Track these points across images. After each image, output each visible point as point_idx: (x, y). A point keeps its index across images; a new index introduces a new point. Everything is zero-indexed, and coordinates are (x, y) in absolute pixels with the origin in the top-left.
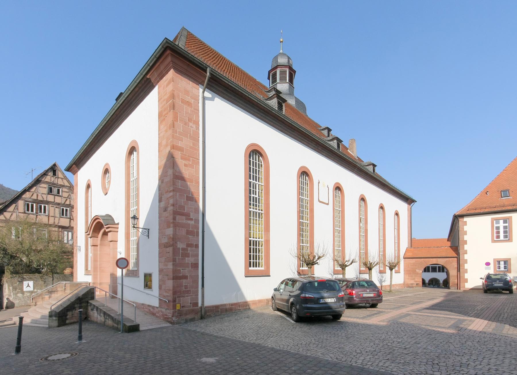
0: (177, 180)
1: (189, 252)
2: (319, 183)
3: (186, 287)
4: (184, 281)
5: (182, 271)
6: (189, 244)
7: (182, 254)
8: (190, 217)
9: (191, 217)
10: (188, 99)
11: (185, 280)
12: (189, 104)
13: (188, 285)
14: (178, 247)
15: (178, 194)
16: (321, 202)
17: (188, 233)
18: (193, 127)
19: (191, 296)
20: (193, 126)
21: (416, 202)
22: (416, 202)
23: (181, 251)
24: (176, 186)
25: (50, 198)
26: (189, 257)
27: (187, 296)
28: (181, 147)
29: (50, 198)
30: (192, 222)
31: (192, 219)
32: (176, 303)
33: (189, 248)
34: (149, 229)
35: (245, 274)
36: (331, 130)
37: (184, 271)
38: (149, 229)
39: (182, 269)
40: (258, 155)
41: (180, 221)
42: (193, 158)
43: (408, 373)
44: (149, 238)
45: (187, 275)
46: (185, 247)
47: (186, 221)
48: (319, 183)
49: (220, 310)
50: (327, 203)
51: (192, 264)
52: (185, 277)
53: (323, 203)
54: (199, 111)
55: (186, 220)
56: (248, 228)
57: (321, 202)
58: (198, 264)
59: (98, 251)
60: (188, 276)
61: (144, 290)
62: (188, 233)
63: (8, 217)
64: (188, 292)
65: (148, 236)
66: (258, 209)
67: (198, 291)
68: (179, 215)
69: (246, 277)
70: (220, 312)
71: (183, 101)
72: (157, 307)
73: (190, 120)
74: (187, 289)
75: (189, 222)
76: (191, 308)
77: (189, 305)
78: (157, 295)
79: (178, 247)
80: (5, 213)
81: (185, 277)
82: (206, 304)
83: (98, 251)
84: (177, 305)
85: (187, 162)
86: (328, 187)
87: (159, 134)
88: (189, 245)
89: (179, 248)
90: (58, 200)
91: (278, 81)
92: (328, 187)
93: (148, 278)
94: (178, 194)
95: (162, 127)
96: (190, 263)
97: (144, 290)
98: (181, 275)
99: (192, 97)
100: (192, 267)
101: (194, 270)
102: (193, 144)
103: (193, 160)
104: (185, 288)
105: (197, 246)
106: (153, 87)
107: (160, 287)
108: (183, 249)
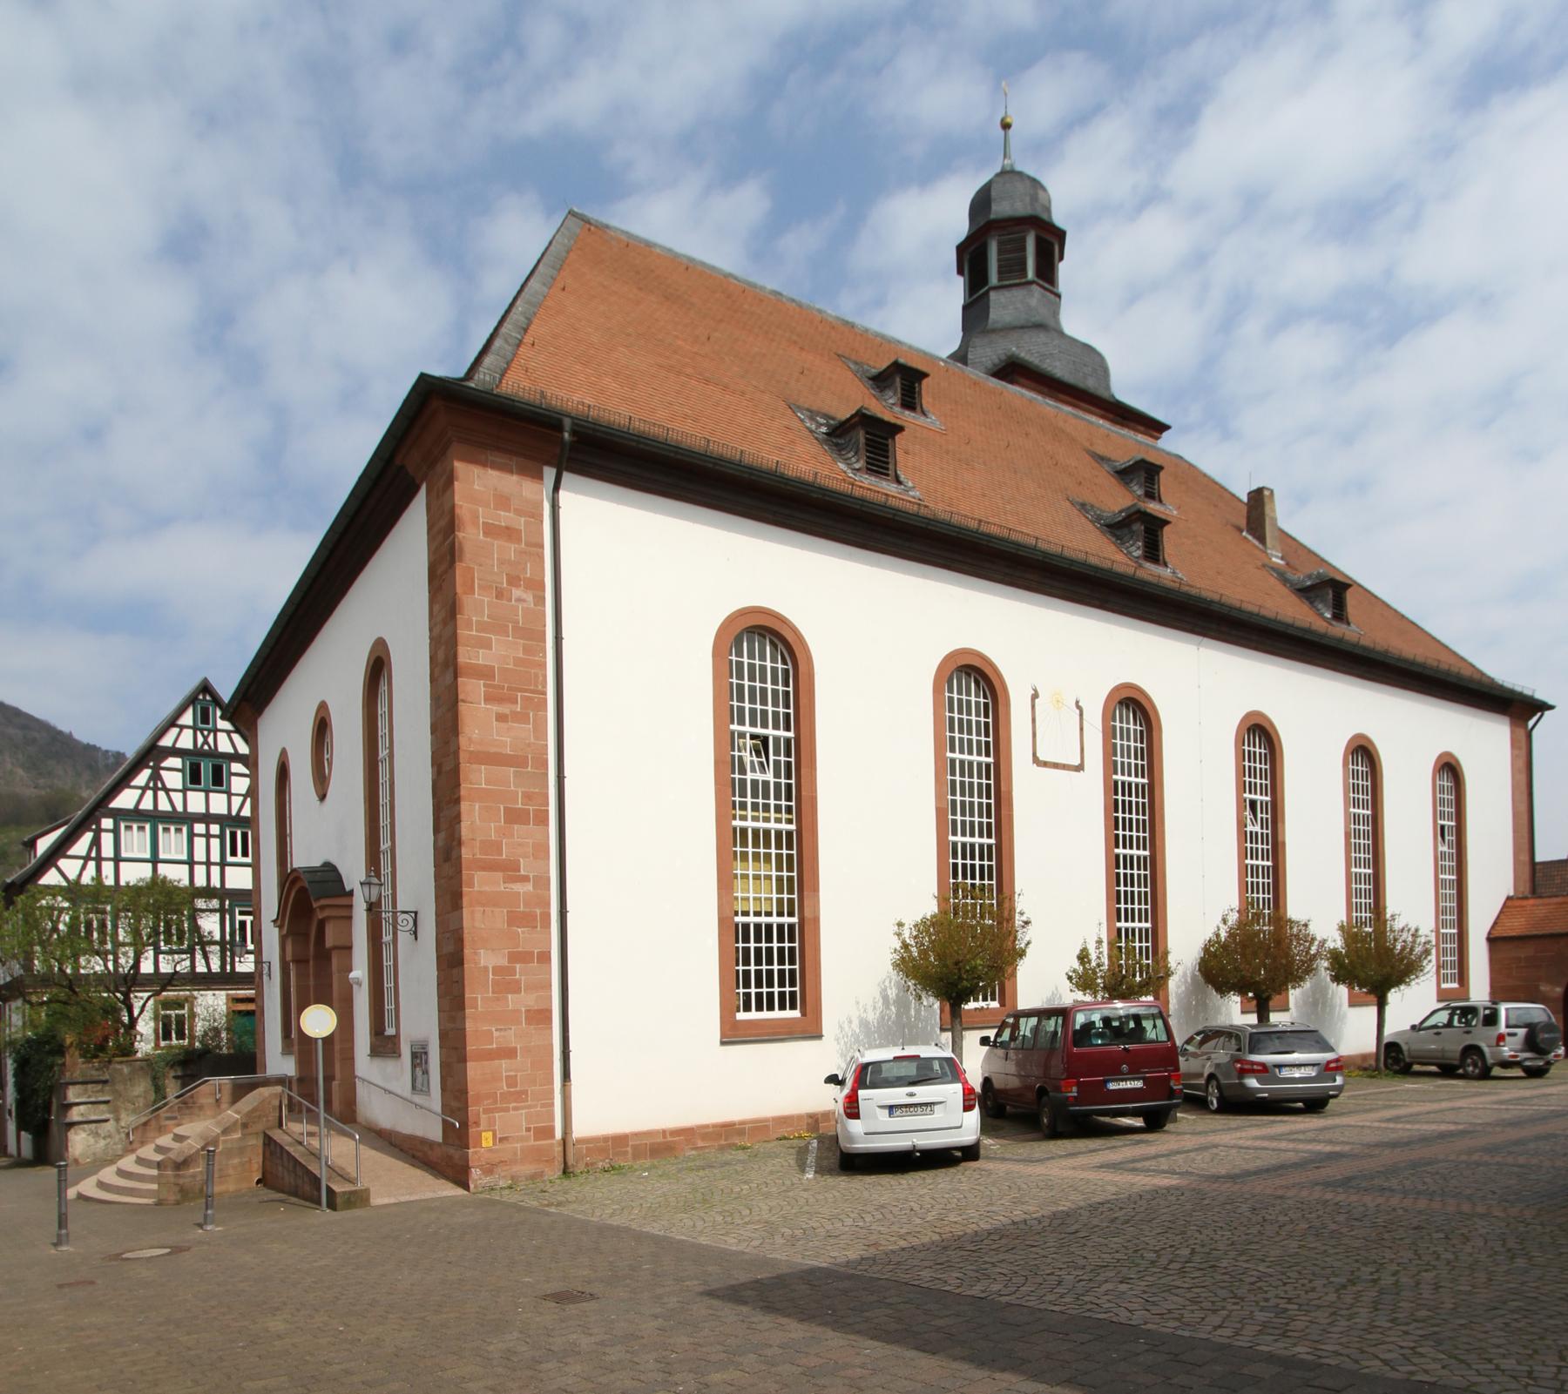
0: (474, 766)
1: (518, 976)
2: (1035, 696)
3: (512, 1081)
4: (504, 1063)
5: (496, 1034)
6: (519, 953)
7: (495, 983)
8: (519, 871)
9: (522, 872)
10: (505, 518)
11: (508, 1061)
12: (510, 533)
13: (519, 1074)
14: (482, 963)
15: (477, 807)
16: (1045, 764)
17: (515, 919)
18: (524, 601)
19: (529, 1107)
20: (524, 596)
21: (1551, 707)
22: (1551, 707)
23: (491, 976)
24: (471, 783)
25: (196, 802)
26: (518, 991)
27: (516, 1109)
28: (486, 666)
29: (196, 802)
30: (529, 887)
31: (525, 879)
32: (481, 1128)
33: (518, 966)
34: (416, 913)
35: (723, 1035)
36: (1161, 468)
37: (502, 1033)
38: (416, 913)
39: (496, 1030)
40: (772, 643)
41: (487, 889)
42: (526, 691)
43: (1400, 1368)
44: (416, 939)
45: (513, 1045)
46: (504, 962)
47: (507, 885)
48: (1035, 696)
49: (629, 1149)
50: (1077, 762)
51: (528, 1011)
52: (510, 1053)
53: (1056, 766)
54: (542, 546)
55: (504, 882)
56: (726, 881)
57: (1045, 764)
58: (550, 1011)
59: (311, 978)
60: (516, 1048)
61: (413, 1094)
62: (515, 919)
63: (72, 876)
64: (520, 1096)
65: (415, 933)
66: (772, 819)
67: (552, 1091)
68: (484, 869)
69: (723, 1043)
70: (630, 1156)
71: (490, 530)
72: (439, 1144)
73: (514, 581)
74: (516, 1086)
75: (518, 887)
76: (532, 1142)
77: (524, 1133)
78: (437, 1107)
79: (482, 963)
80: (62, 863)
81: (510, 1053)
82: (580, 1130)
83: (311, 978)
84: (483, 1134)
85: (505, 709)
86: (1078, 706)
87: (431, 630)
88: (518, 957)
89: (486, 968)
90: (218, 804)
91: (994, 279)
92: (1078, 706)
93: (419, 1057)
94: (477, 807)
95: (436, 608)
96: (523, 1009)
97: (413, 1094)
98: (495, 1046)
99: (519, 512)
100: (529, 1020)
101: (535, 1029)
102: (527, 650)
103: (525, 699)
104: (509, 1086)
105: (545, 957)
106: (414, 491)
107: (443, 1090)
108: (497, 970)
